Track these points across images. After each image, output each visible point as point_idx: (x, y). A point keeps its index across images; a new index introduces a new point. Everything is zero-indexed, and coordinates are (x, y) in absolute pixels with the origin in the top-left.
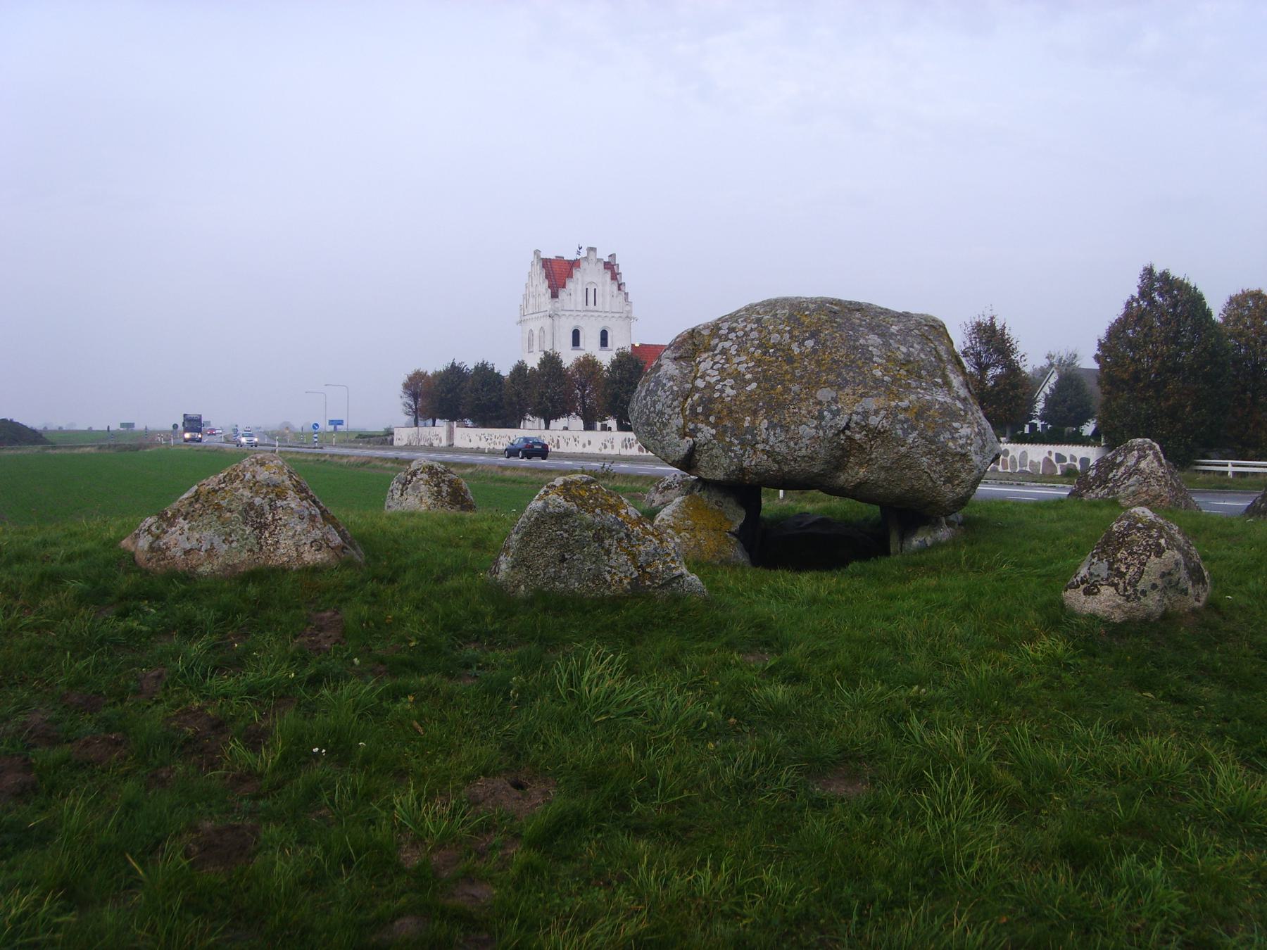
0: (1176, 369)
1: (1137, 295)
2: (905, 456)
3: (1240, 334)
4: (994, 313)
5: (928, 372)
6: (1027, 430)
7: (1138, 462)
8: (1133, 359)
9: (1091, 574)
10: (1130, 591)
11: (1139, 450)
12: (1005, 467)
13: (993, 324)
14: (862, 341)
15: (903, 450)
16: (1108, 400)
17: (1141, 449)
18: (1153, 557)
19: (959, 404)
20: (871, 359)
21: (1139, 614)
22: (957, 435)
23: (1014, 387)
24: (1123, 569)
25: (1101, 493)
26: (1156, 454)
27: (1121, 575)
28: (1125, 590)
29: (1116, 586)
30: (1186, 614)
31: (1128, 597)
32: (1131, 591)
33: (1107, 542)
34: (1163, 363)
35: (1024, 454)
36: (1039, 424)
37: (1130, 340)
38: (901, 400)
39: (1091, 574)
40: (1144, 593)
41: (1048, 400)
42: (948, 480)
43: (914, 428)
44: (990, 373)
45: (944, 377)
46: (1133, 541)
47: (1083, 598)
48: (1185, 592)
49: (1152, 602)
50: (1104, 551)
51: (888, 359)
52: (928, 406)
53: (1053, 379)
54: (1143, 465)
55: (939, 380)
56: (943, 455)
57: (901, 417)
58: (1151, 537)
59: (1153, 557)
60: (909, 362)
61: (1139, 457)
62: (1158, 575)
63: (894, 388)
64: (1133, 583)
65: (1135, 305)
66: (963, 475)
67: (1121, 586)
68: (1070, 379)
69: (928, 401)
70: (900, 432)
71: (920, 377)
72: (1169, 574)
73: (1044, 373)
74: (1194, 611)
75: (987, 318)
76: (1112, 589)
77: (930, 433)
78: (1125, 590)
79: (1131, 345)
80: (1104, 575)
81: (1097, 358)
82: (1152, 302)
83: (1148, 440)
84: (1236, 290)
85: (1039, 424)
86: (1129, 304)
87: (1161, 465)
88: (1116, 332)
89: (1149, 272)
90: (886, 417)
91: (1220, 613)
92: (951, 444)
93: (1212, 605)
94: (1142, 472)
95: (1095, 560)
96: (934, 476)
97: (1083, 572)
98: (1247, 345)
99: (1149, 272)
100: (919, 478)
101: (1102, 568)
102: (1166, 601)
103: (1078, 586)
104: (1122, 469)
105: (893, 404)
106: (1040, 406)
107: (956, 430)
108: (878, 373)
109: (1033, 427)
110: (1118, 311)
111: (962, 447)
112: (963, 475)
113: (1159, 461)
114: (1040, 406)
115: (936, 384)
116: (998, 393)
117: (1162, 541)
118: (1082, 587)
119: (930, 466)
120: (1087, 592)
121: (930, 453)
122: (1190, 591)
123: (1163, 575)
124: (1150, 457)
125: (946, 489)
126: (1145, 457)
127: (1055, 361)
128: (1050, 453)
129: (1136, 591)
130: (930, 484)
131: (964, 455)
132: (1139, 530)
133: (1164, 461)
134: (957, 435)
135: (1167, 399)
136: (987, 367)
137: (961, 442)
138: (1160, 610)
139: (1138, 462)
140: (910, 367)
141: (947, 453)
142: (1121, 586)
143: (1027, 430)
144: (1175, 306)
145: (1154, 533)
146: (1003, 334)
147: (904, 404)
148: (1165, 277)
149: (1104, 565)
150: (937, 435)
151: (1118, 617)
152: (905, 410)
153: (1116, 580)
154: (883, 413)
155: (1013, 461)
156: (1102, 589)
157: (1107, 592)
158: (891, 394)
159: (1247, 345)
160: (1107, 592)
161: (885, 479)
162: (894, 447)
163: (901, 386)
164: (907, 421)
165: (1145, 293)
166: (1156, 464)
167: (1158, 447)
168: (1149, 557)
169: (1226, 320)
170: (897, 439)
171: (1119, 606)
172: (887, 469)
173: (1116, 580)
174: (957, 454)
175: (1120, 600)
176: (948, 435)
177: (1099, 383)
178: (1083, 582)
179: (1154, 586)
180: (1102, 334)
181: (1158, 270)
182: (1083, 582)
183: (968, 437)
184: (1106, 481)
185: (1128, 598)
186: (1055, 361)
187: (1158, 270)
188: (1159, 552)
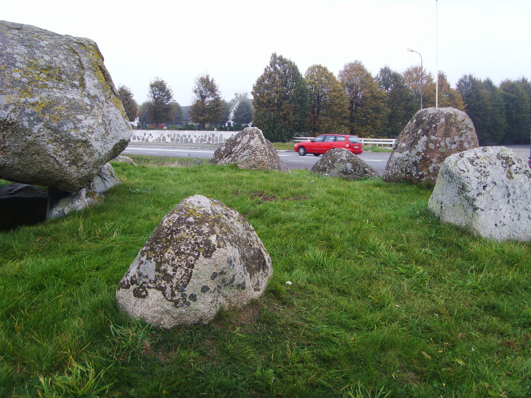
0: (286, 98)
1: (269, 66)
2: (32, 144)
3: (313, 83)
4: (208, 74)
5: (68, 76)
6: (227, 125)
7: (249, 141)
8: (268, 94)
9: (140, 274)
10: (178, 296)
11: (250, 134)
12: (213, 141)
13: (208, 79)
14: (9, 50)
15: (30, 138)
16: (257, 111)
17: (252, 133)
18: (201, 258)
19: (87, 100)
20: (13, 65)
21: (190, 319)
22: (79, 125)
23: (217, 106)
24: (170, 272)
25: (227, 160)
26: (260, 137)
27: (169, 278)
28: (173, 295)
29: (162, 289)
30: (244, 308)
31: (176, 303)
32: (180, 296)
33: (156, 240)
34: (280, 96)
35: (221, 135)
36: (232, 122)
37: (266, 85)
38: (33, 97)
39: (140, 274)
40: (193, 297)
41: (236, 114)
42: (74, 163)
43: (39, 120)
44: (207, 99)
45: (82, 80)
46: (181, 239)
47: (133, 299)
48: (242, 287)
49: (205, 307)
50: (152, 249)
51: (30, 65)
52: (58, 101)
53: (237, 104)
54: (252, 143)
55: (77, 83)
56: (67, 142)
57: (28, 111)
58: (200, 233)
59: (201, 258)
60: (51, 68)
61: (250, 138)
62: (209, 276)
63: (30, 88)
64: (181, 287)
65: (268, 70)
66: (86, 158)
67: (168, 290)
68: (244, 105)
69: (57, 98)
70: (26, 124)
71: (60, 80)
72: (222, 273)
73: (234, 101)
74: (253, 303)
75: (205, 76)
76: (159, 293)
77: (55, 124)
78: (173, 295)
79: (267, 87)
80: (152, 277)
81: (252, 93)
82: (275, 69)
83: (256, 128)
84: (311, 65)
85: (232, 122)
86: (266, 70)
87: (263, 143)
88: (260, 82)
89: (274, 56)
90: (14, 111)
91: (280, 299)
92: (73, 133)
93: (273, 292)
94: (251, 147)
95: (144, 259)
96: (60, 160)
97: (133, 270)
98: (315, 88)
99: (274, 56)
100: (47, 162)
101: (150, 269)
102: (221, 299)
103: (128, 287)
104: (240, 146)
105: (23, 100)
106: (232, 115)
107: (80, 121)
108: (17, 76)
109: (229, 124)
110: (261, 73)
111: (83, 135)
112: (86, 158)
113: (262, 140)
114: (232, 115)
115: (73, 86)
116: (210, 109)
117: (213, 238)
118: (132, 287)
119: (55, 152)
120: (137, 294)
121: (55, 141)
122: (249, 283)
123: (214, 276)
124: (257, 138)
125: (73, 170)
126: (253, 138)
127: (238, 96)
128: (232, 135)
129: (184, 296)
130: (57, 166)
131: (85, 142)
132: (189, 224)
133: (265, 140)
134: (79, 125)
135: (283, 111)
136: (205, 97)
137: (82, 131)
138: (214, 311)
139: (249, 141)
140: (51, 72)
141: (70, 140)
142: (168, 290)
143: (227, 125)
144: (285, 71)
145: (205, 229)
146: (212, 83)
147: (31, 100)
148: (281, 58)
149: (152, 265)
150: (61, 125)
151: (167, 323)
152: (33, 105)
153: (163, 283)
154: (12, 107)
155: (217, 139)
156: (151, 292)
157: (154, 295)
158: (25, 91)
159: (315, 88)
160: (154, 295)
161: (20, 164)
162: (23, 136)
163: (37, 86)
164: (33, 114)
165: (273, 64)
166: (260, 142)
167: (261, 132)
168: (197, 258)
169: (307, 77)
170: (24, 129)
171: (167, 312)
172: (20, 155)
173: (163, 283)
174: (78, 141)
175: (168, 306)
176: (71, 125)
177: (253, 104)
178: (133, 282)
179: (205, 289)
180: (255, 83)
181: (278, 55)
182: (133, 282)
183: (90, 127)
184: (231, 153)
185: (176, 304)
186: (238, 96)
187: (278, 55)
188: (209, 251)
